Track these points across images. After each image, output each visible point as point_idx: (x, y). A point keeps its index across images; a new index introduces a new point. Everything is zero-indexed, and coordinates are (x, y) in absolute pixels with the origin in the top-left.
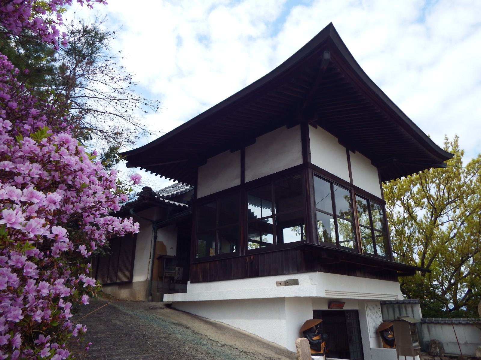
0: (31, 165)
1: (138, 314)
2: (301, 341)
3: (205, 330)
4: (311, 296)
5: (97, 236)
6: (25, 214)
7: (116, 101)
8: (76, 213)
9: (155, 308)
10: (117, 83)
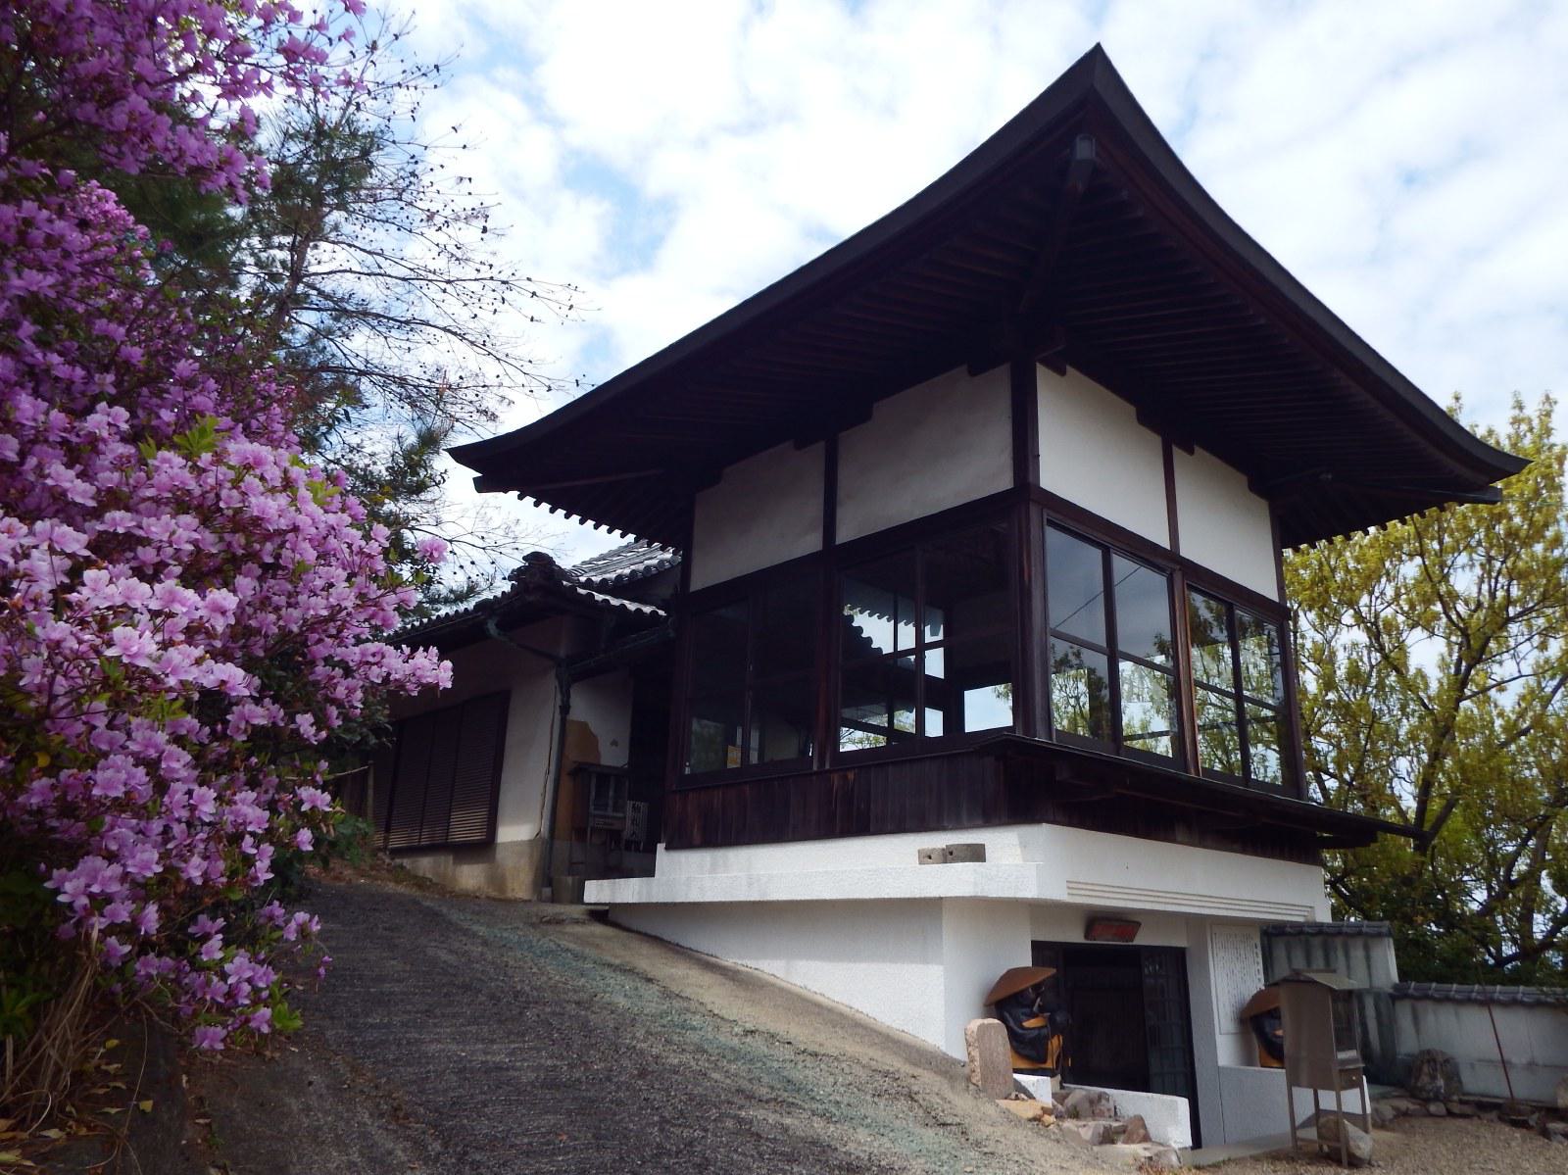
0: (174, 521)
1: (505, 935)
2: (981, 1027)
3: (701, 987)
4: (1020, 895)
5: (341, 692)
6: (159, 637)
7: (443, 285)
8: (285, 634)
9: (558, 921)
10: (444, 228)
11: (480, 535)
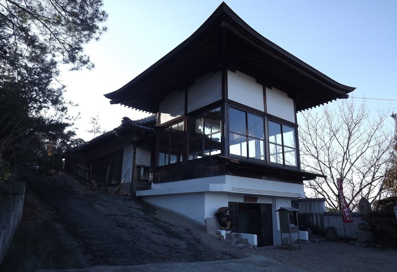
11: (316, 115)
